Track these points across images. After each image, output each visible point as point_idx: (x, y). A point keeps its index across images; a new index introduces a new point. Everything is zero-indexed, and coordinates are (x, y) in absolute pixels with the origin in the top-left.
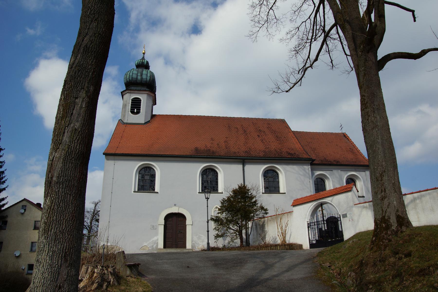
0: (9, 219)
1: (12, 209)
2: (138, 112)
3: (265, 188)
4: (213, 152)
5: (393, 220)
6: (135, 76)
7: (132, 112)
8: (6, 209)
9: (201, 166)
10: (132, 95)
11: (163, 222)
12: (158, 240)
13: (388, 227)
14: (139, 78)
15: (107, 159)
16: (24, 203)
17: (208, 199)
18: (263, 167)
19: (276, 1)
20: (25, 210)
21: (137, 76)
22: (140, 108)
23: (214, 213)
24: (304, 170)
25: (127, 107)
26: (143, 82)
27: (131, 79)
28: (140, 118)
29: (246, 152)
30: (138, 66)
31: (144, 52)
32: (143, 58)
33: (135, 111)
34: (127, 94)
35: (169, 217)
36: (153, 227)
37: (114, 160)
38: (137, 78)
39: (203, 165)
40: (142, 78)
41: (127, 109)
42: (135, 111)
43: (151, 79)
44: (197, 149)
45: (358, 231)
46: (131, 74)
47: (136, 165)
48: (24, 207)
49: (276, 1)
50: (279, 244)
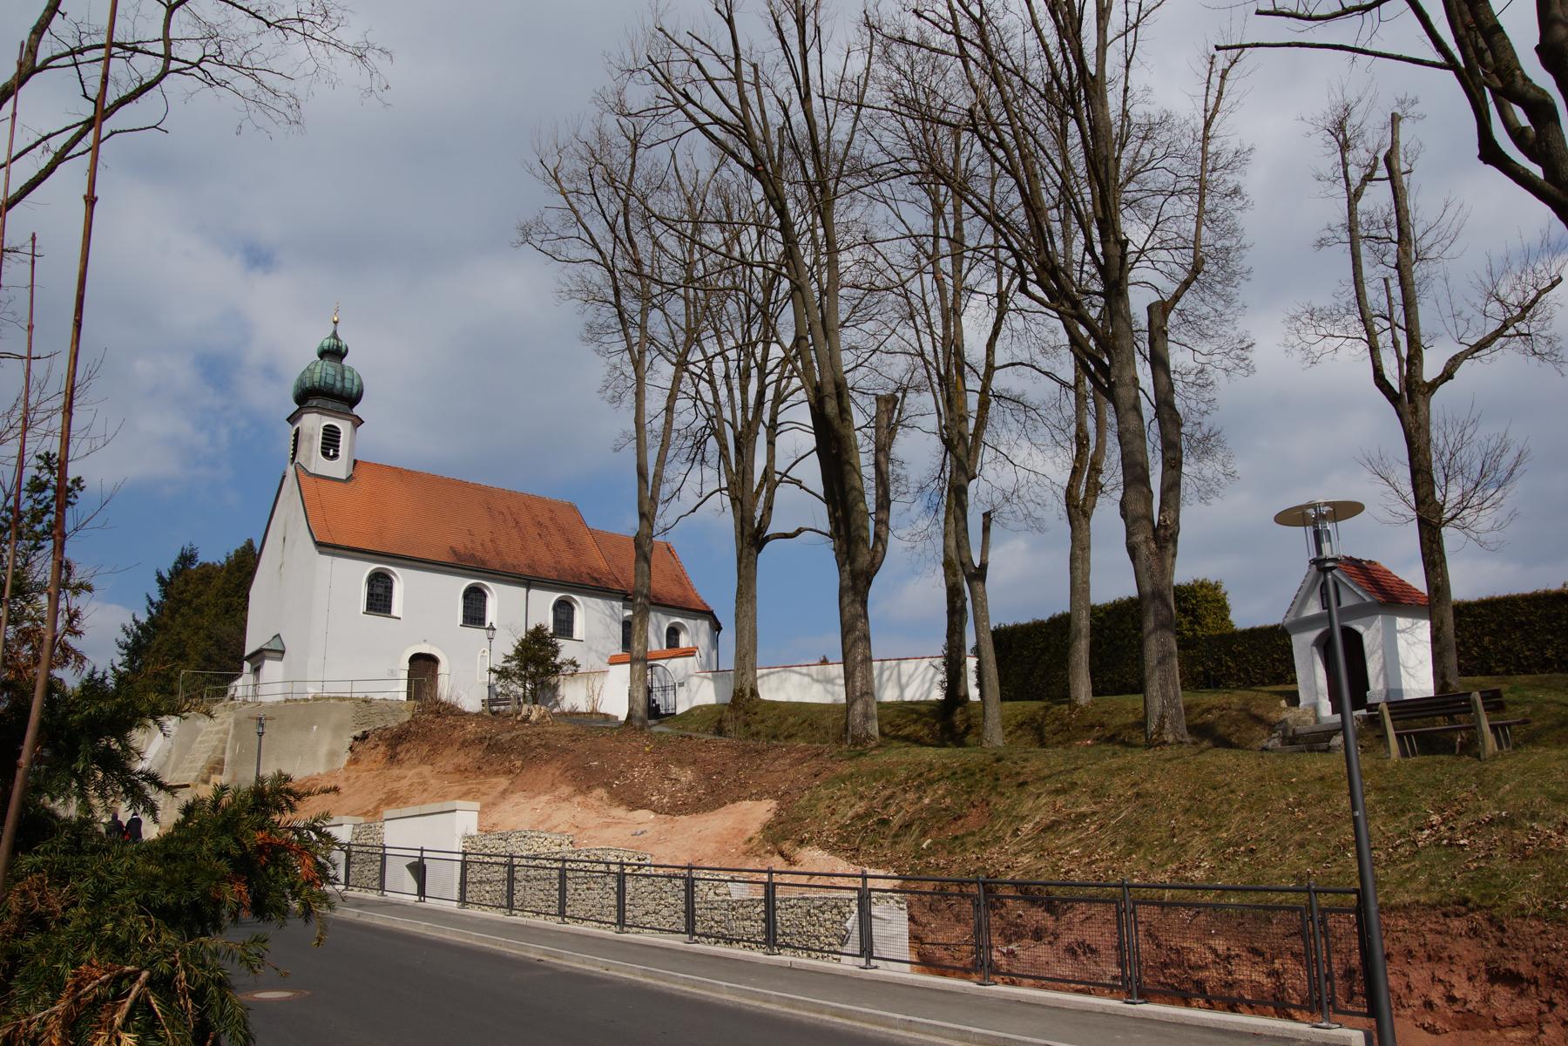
2: (335, 456)
3: (1392, 720)
4: (483, 562)
5: (748, 692)
6: (330, 380)
7: (325, 454)
9: (555, 596)
10: (324, 418)
11: (407, 666)
13: (743, 696)
14: (339, 385)
15: (321, 553)
17: (491, 639)
18: (555, 596)
19: (53, 9)
23: (498, 662)
24: (612, 608)
28: (338, 468)
29: (529, 566)
32: (335, 336)
37: (333, 555)
39: (557, 595)
44: (455, 552)
45: (695, 704)
49: (53, 9)
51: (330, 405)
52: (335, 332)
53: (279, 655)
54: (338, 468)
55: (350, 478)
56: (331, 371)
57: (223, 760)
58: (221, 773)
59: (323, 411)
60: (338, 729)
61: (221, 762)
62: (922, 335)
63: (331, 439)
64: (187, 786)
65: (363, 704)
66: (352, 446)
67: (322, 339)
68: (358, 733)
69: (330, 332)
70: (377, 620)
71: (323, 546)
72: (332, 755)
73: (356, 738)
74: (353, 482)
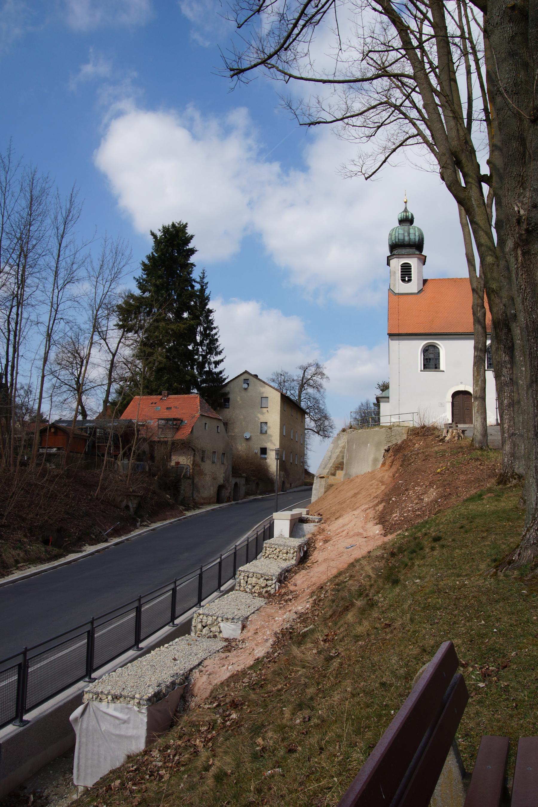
0: (231, 396)
1: (232, 383)
2: (410, 280)
6: (401, 237)
7: (403, 280)
8: (229, 382)
11: (450, 399)
12: (446, 416)
14: (407, 238)
15: (392, 340)
16: (246, 376)
20: (248, 384)
21: (404, 236)
22: (411, 274)
25: (397, 275)
26: (411, 243)
27: (397, 240)
28: (413, 287)
30: (402, 221)
31: (405, 200)
32: (406, 211)
33: (407, 279)
34: (395, 259)
35: (456, 395)
36: (441, 404)
37: (399, 339)
38: (404, 239)
40: (410, 239)
41: (397, 277)
42: (407, 279)
43: (421, 239)
46: (397, 235)
47: (421, 344)
48: (246, 381)
50: (486, 513)
51: (404, 251)
52: (406, 208)
53: (386, 399)
54: (413, 287)
55: (419, 292)
56: (401, 232)
57: (343, 462)
58: (342, 469)
59: (400, 256)
60: (378, 445)
61: (342, 464)
62: (5, 186)
63: (406, 271)
64: (323, 477)
65: (389, 430)
66: (420, 272)
67: (398, 214)
68: (386, 448)
69: (403, 209)
70: (431, 375)
71: (391, 335)
72: (375, 460)
73: (385, 450)
74: (423, 293)
